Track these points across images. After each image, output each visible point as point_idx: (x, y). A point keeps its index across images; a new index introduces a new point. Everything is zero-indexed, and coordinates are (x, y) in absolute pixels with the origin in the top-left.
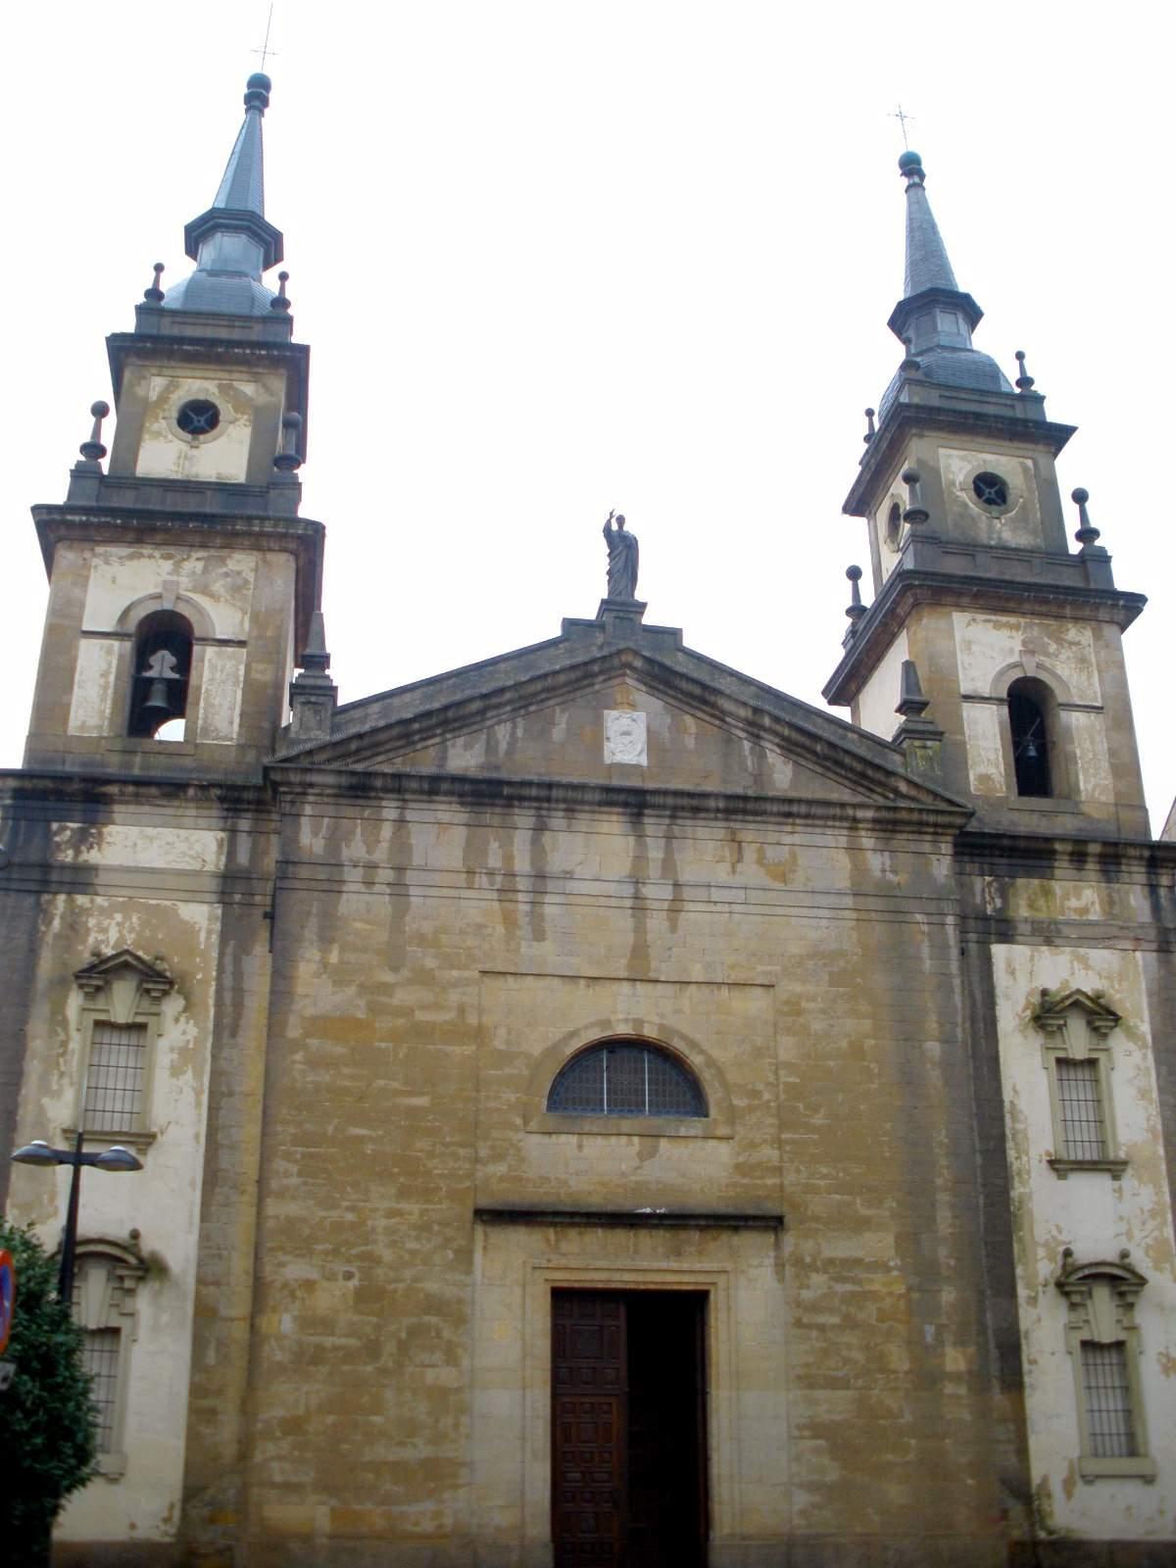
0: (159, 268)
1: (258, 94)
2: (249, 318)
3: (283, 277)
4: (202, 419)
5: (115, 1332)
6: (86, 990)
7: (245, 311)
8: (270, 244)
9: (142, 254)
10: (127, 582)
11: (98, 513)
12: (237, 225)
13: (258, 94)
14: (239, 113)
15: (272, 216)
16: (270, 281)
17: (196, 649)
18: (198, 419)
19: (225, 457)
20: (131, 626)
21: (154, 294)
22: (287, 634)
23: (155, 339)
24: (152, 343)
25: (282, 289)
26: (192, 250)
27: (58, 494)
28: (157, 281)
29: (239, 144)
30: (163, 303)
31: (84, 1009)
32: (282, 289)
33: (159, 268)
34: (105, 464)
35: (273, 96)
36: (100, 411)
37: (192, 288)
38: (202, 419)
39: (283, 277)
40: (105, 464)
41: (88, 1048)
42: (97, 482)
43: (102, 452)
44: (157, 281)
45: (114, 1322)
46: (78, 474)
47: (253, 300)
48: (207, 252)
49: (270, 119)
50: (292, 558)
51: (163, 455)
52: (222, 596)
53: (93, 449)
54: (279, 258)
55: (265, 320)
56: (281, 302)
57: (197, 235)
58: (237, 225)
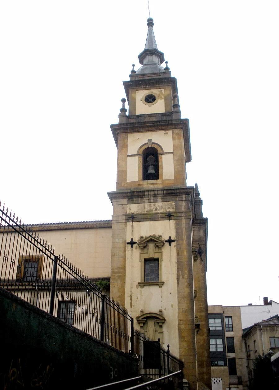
0: (133, 65)
1: (150, 23)
2: (159, 73)
3: (167, 63)
4: (151, 99)
5: (157, 260)
6: (141, 247)
7: (158, 72)
8: (161, 56)
9: (129, 63)
10: (137, 142)
11: (127, 126)
12: (151, 53)
13: (150, 23)
14: (146, 28)
15: (160, 49)
16: (163, 66)
17: (160, 156)
18: (150, 99)
19: (159, 107)
20: (141, 152)
21: (133, 72)
22: (195, 305)
23: (136, 81)
24: (134, 84)
25: (167, 65)
26: (141, 62)
27: (116, 121)
28: (133, 68)
29: (148, 35)
30: (136, 73)
31: (141, 253)
32: (167, 65)
33: (133, 65)
34: (127, 113)
35: (154, 22)
36: (123, 101)
37: (142, 69)
38: (151, 99)
39: (167, 63)
40: (127, 113)
41: (154, 332)
42: (126, 118)
43: (125, 110)
44: (133, 68)
45: (156, 256)
46: (120, 116)
47: (160, 69)
48: (145, 62)
49: (155, 28)
50: (182, 130)
51: (142, 109)
52: (164, 140)
53: (123, 110)
54: (163, 60)
55: (164, 73)
56: (167, 69)
57: (142, 58)
58: (151, 53)
